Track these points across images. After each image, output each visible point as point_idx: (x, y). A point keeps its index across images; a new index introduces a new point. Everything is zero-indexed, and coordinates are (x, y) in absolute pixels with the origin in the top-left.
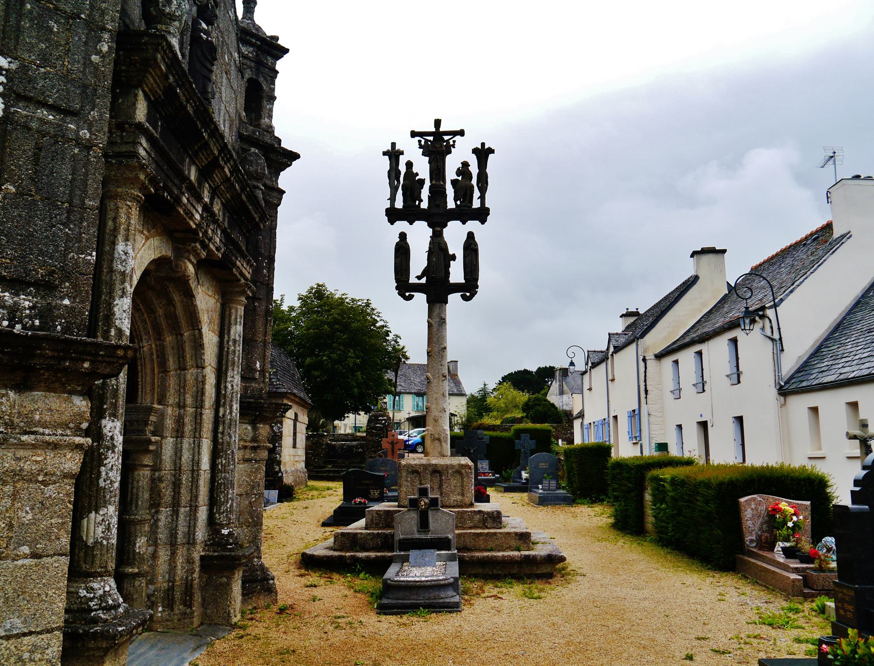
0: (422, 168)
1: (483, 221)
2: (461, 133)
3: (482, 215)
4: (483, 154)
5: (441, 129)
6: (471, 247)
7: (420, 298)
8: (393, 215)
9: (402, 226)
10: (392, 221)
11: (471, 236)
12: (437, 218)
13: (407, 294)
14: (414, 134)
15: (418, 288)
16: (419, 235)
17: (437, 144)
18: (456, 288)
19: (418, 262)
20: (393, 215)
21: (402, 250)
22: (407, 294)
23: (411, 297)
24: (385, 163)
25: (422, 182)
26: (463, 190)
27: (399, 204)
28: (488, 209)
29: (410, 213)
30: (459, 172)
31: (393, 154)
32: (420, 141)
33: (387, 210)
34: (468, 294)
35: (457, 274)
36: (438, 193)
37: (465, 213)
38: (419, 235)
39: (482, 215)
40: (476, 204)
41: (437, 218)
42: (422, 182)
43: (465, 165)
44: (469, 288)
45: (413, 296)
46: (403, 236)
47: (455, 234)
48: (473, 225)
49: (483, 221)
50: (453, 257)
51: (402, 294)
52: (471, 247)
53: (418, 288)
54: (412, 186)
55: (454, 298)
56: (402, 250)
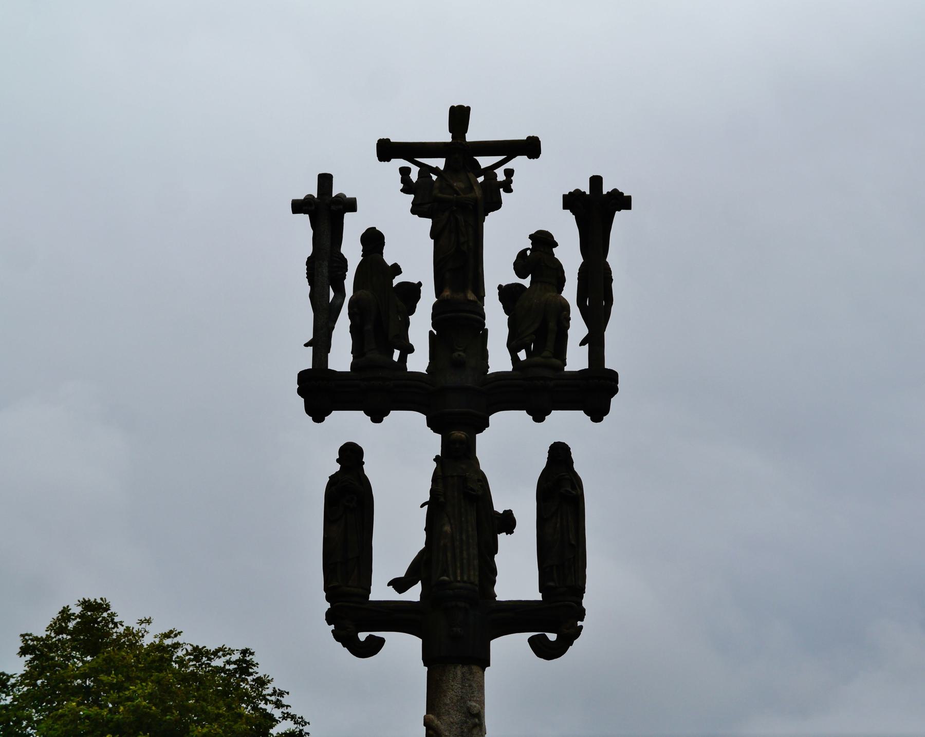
0: (413, 251)
1: (598, 413)
2: (530, 147)
3: (594, 392)
4: (596, 209)
5: (472, 136)
6: (560, 488)
7: (403, 650)
8: (321, 392)
9: (348, 424)
10: (317, 411)
11: (560, 454)
12: (458, 403)
13: (362, 636)
14: (387, 150)
15: (396, 617)
16: (402, 453)
17: (456, 180)
18: (515, 617)
19: (398, 537)
20: (321, 392)
21: (349, 499)
22: (362, 636)
23: (372, 648)
24: (301, 234)
25: (412, 292)
26: (536, 317)
27: (341, 357)
28: (613, 377)
29: (374, 387)
30: (522, 264)
31: (325, 209)
32: (405, 172)
33: (303, 377)
34: (552, 637)
35: (517, 573)
36: (459, 325)
37: (542, 387)
38: (402, 453)
39: (594, 392)
40: (577, 359)
41: (458, 403)
42: (412, 292)
43: (543, 241)
44: (556, 618)
45: (381, 641)
46: (351, 456)
47: (511, 450)
48: (567, 424)
49: (598, 413)
50: (507, 522)
51: (345, 637)
52: (560, 488)
53: (396, 617)
54: (381, 302)
55: (510, 650)
56: (349, 499)
